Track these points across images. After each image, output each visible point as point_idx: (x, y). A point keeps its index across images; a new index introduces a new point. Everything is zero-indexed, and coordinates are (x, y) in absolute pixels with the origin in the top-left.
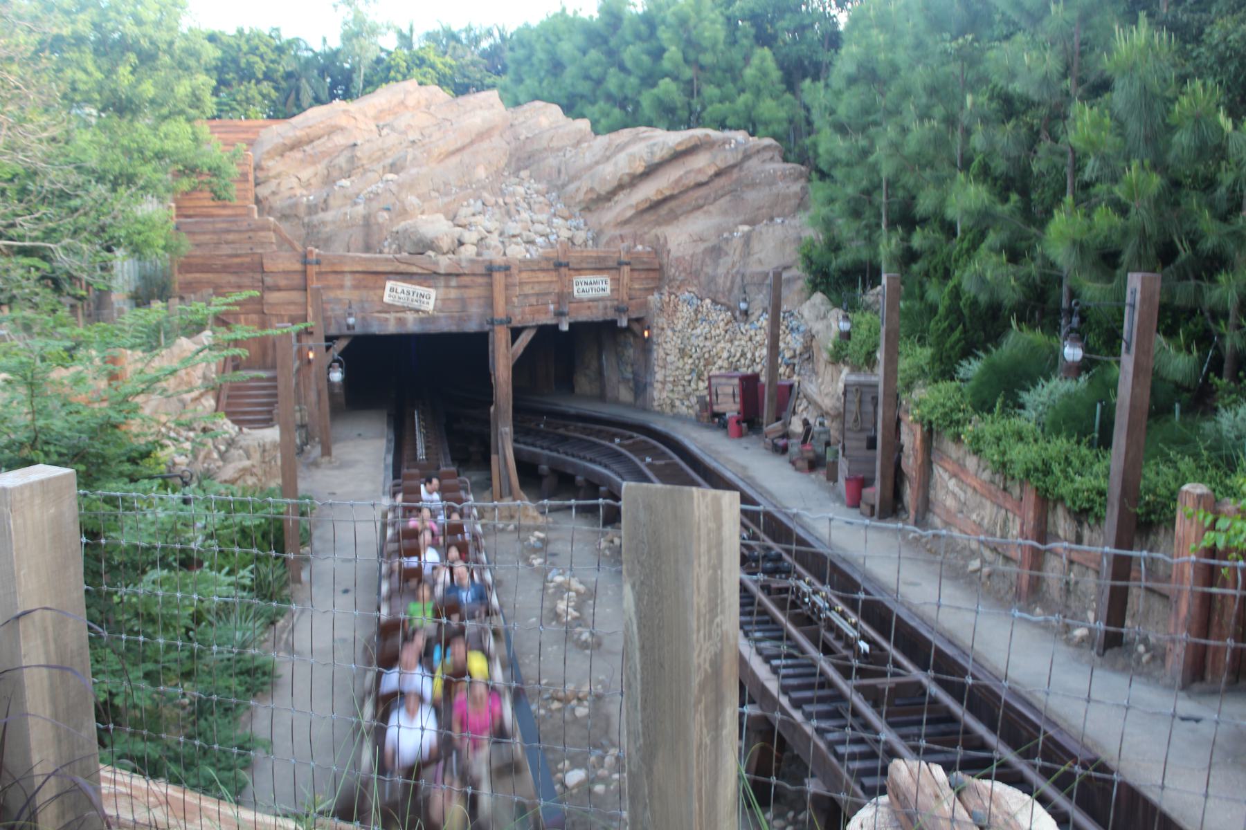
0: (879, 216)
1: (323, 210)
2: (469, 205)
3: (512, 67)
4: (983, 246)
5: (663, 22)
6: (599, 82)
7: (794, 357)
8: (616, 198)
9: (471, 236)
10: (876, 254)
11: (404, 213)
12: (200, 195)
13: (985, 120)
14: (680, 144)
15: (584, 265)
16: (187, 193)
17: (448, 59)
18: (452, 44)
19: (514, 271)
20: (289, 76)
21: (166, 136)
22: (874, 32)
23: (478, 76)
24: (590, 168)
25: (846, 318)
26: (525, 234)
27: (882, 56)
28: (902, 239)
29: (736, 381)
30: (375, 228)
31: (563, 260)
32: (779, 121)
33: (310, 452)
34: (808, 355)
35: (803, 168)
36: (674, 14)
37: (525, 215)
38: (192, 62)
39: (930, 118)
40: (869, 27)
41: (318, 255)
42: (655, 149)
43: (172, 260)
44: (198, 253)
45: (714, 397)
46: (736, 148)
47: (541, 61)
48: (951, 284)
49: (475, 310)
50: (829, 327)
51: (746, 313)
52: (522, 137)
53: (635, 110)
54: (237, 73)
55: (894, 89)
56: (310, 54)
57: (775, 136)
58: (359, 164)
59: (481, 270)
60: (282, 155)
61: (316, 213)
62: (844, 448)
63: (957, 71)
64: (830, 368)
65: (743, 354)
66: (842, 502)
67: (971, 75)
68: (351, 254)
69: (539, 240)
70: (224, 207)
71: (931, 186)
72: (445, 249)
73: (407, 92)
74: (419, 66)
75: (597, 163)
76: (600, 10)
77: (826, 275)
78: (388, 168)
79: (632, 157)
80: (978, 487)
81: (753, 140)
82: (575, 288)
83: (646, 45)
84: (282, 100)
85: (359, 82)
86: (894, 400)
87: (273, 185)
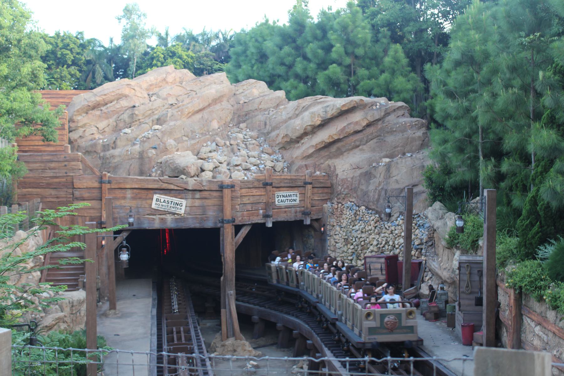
0: (477, 151)
1: (113, 148)
2: (207, 146)
3: (234, 57)
4: (552, 170)
5: (332, 28)
6: (290, 67)
7: (421, 244)
8: (302, 141)
9: (209, 166)
10: (477, 176)
11: (166, 150)
12: (33, 138)
13: (552, 87)
14: (344, 106)
15: (282, 185)
16: (26, 136)
17: (190, 53)
18: (193, 43)
19: (237, 188)
20: (88, 62)
21: (15, 99)
22: (472, 32)
23: (210, 63)
24: (285, 121)
25: (460, 218)
26: (244, 164)
27: (478, 48)
28: (495, 166)
29: (383, 260)
30: (147, 160)
31: (269, 181)
32: (407, 91)
33: (101, 307)
34: (431, 242)
35: (424, 121)
36: (338, 23)
37: (244, 152)
38: (33, 53)
39: (512, 87)
40: (469, 29)
41: (109, 177)
42: (328, 109)
43: (13, 180)
44: (31, 175)
45: (368, 271)
46: (380, 108)
47: (252, 53)
48: (530, 195)
49: (211, 213)
50: (445, 224)
51: (389, 215)
52: (241, 102)
53: (313, 85)
54: (55, 61)
55: (485, 69)
56: (102, 49)
57: (404, 100)
58: (137, 118)
59: (216, 187)
60: (87, 113)
61: (108, 150)
62: (460, 305)
63: (529, 56)
64: (447, 251)
65: (387, 242)
66: (460, 342)
67: (538, 58)
68: (130, 177)
69: (253, 168)
70: (49, 146)
71: (514, 131)
72: (192, 174)
73: (168, 73)
74: (172, 57)
75: (290, 118)
76: (291, 21)
77: (442, 190)
78: (155, 122)
79: (313, 115)
80: (556, 331)
81: (392, 104)
82: (277, 199)
83: (320, 43)
84: (84, 78)
85: (133, 67)
86: (493, 271)
87: (80, 132)
